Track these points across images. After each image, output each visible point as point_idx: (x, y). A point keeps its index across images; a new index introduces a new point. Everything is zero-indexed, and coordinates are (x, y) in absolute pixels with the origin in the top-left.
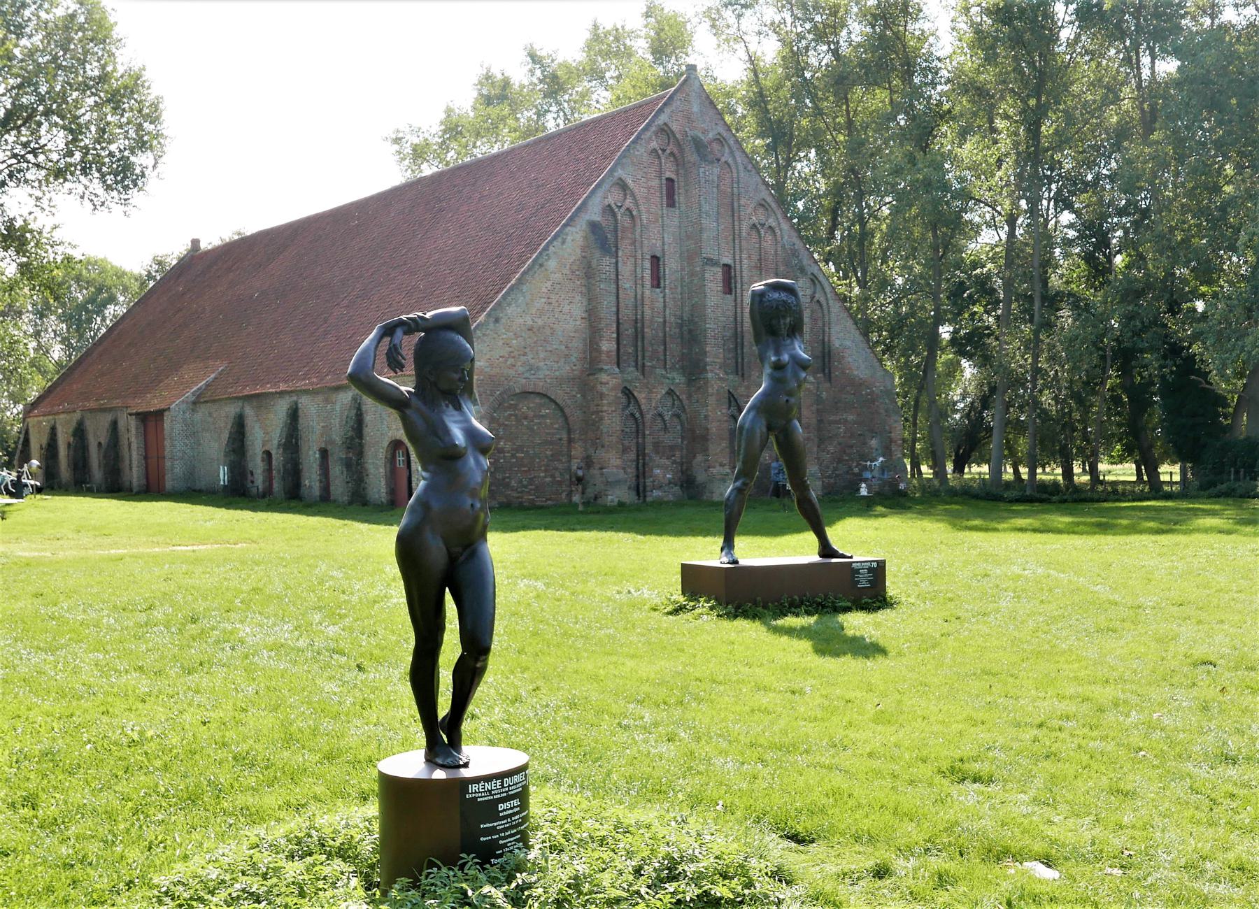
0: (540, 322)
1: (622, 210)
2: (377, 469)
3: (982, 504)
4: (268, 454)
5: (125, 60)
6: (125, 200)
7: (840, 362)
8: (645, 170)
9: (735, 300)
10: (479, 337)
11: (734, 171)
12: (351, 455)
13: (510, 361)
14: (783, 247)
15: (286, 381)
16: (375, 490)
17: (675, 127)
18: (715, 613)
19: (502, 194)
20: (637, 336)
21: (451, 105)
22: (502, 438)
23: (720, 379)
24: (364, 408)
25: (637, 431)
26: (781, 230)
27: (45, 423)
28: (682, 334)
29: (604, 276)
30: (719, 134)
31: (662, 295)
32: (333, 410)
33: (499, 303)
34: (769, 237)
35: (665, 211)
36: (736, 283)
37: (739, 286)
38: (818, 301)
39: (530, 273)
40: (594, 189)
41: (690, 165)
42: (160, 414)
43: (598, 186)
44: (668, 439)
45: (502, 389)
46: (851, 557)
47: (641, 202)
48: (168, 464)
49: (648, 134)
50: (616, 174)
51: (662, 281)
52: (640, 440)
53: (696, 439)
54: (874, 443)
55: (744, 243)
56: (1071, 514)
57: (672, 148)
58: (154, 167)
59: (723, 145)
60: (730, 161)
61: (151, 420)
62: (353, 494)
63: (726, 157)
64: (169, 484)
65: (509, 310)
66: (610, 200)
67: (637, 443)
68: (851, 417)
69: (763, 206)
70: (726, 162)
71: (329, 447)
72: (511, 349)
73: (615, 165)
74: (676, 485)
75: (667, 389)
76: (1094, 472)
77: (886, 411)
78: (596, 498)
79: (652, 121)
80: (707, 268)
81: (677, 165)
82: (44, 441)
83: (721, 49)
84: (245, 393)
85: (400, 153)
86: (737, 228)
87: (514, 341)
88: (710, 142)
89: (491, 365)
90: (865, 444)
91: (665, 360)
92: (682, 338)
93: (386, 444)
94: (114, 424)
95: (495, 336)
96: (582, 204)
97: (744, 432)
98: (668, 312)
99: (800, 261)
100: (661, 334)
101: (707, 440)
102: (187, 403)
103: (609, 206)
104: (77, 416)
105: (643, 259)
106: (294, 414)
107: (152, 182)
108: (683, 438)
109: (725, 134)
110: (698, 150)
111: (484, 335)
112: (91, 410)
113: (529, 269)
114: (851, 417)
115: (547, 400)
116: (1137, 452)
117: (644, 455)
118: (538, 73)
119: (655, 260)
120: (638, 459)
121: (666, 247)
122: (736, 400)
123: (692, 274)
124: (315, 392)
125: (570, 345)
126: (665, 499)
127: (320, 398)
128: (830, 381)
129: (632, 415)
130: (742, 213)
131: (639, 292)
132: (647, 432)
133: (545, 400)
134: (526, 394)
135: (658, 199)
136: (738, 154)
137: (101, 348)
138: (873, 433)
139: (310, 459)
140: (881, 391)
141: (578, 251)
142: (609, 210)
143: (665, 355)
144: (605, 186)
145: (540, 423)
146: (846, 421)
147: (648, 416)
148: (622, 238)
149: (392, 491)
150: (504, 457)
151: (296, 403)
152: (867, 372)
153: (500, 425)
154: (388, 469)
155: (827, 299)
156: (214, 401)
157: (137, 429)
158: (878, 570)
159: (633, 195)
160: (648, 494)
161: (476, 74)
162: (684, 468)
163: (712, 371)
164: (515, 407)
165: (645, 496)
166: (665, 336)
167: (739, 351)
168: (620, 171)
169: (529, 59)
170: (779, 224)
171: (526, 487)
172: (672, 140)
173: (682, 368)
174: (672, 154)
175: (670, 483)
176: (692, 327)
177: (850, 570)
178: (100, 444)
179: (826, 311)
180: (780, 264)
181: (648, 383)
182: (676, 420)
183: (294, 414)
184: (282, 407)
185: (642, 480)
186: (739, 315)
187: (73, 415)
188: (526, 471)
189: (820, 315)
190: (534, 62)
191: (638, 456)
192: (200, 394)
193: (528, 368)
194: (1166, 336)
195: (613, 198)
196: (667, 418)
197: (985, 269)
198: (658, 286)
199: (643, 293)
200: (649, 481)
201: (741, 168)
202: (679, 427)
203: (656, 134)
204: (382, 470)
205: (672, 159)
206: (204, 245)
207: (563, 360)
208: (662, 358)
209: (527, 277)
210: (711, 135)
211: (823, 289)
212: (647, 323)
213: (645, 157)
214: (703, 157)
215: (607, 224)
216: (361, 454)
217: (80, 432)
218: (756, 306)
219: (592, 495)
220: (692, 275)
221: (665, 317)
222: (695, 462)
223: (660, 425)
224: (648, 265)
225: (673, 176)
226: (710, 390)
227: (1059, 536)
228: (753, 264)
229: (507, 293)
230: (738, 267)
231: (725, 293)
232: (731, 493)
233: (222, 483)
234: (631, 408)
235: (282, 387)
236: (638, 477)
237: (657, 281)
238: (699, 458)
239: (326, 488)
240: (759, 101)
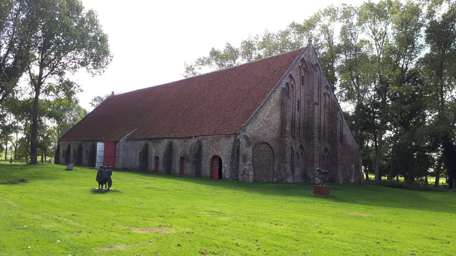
10: (251, 123)
14: (332, 101)
17: (305, 59)
26: (331, 95)
27: (67, 143)
29: (288, 105)
57: (304, 66)
66: (288, 81)
80: (315, 105)
81: (305, 72)
82: (66, 149)
86: (320, 93)
92: (304, 128)
93: (211, 157)
101: (314, 162)
109: (318, 63)
124: (180, 138)
125: (275, 128)
131: (294, 112)
132: (295, 158)
133: (267, 146)
134: (263, 143)
139: (177, 159)
153: (255, 153)
161: (210, 50)
164: (259, 147)
168: (291, 72)
170: (331, 93)
174: (304, 68)
178: (87, 151)
195: (288, 81)
201: (322, 74)
205: (303, 70)
220: (309, 107)
221: (300, 120)
224: (297, 103)
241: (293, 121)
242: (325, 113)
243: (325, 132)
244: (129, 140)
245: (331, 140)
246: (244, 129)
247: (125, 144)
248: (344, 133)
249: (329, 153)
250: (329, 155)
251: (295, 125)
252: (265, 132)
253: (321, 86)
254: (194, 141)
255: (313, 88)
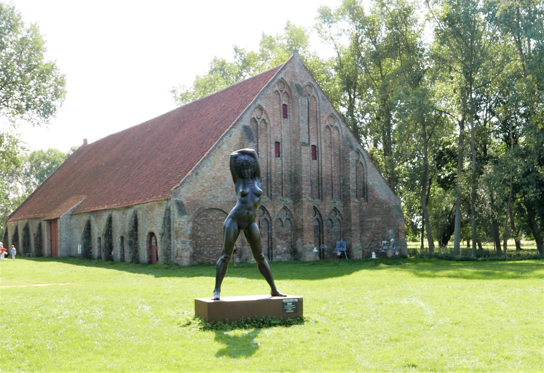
0: (219, 175)
1: (260, 120)
2: (143, 246)
3: (443, 262)
4: (100, 238)
5: (47, 58)
6: (47, 121)
7: (372, 192)
8: (272, 101)
9: (318, 162)
10: (188, 182)
11: (317, 100)
12: (132, 239)
13: (204, 194)
14: (342, 136)
15: (108, 204)
16: (143, 256)
17: (287, 80)
18: (199, 327)
19: (209, 114)
20: (268, 180)
21: (198, 75)
22: (199, 231)
23: (309, 201)
24: (138, 217)
25: (268, 228)
26: (341, 128)
28: (291, 180)
30: (309, 82)
31: (281, 161)
32: (126, 218)
33: (198, 166)
34: (335, 132)
35: (282, 120)
36: (318, 154)
37: (320, 156)
38: (361, 162)
39: (214, 151)
40: (246, 110)
41: (295, 97)
42: (56, 220)
43: (248, 109)
44: (284, 231)
45: (199, 207)
46: (285, 296)
47: (270, 116)
48: (59, 243)
49: (273, 83)
50: (257, 103)
51: (281, 154)
52: (270, 231)
53: (298, 230)
54: (390, 232)
55: (322, 135)
56: (475, 268)
57: (285, 89)
58: (61, 106)
59: (312, 88)
60: (315, 95)
61: (52, 222)
62: (133, 258)
63: (313, 93)
64: (59, 253)
65: (203, 169)
66: (254, 115)
67: (268, 233)
68: (378, 219)
69: (332, 116)
70: (313, 96)
71: (124, 236)
72: (204, 188)
73: (257, 99)
74: (288, 253)
75: (283, 206)
76: (518, 244)
77: (396, 216)
78: (246, 260)
79: (275, 77)
80: (303, 147)
81: (289, 98)
83: (323, 43)
84: (91, 210)
85: (175, 97)
86: (319, 127)
87: (206, 184)
88: (305, 86)
89: (194, 196)
90: (386, 232)
91: (282, 192)
93: (147, 234)
94: (40, 225)
95: (196, 181)
96: (240, 117)
97: (226, 230)
98: (283, 169)
99: (351, 143)
100: (280, 180)
102: (68, 215)
103: (254, 118)
104: (26, 221)
105: (271, 143)
106: (110, 220)
107: (59, 113)
108: (292, 230)
109: (312, 82)
110: (298, 90)
111: (191, 181)
112: (31, 219)
113: (213, 149)
114: (378, 219)
115: (222, 212)
116: (532, 234)
117: (272, 238)
118: (238, 57)
119: (277, 144)
120: (269, 240)
121: (283, 138)
122: (318, 211)
123: (296, 150)
126: (283, 260)
127: (121, 212)
128: (367, 201)
129: (266, 219)
130: (321, 120)
131: (269, 160)
132: (273, 227)
134: (211, 209)
135: (279, 114)
136: (319, 92)
137: (41, 190)
138: (390, 227)
139: (117, 241)
140: (394, 206)
141: (238, 140)
142: (254, 120)
143: (282, 190)
144: (252, 109)
145: (218, 223)
146: (376, 221)
147: (274, 220)
148: (261, 133)
149: (150, 257)
150: (201, 240)
151: (111, 215)
152: (386, 197)
154: (148, 246)
155: (365, 161)
156: (79, 214)
157: (47, 227)
158: (298, 304)
159: (266, 113)
160: (274, 257)
161: (211, 59)
162: (292, 245)
163: (305, 197)
165: (272, 259)
166: (282, 181)
167: (320, 187)
169: (234, 51)
171: (212, 254)
172: (286, 86)
173: (291, 196)
174: (286, 93)
175: (285, 252)
176: (296, 176)
177: (282, 304)
178: (34, 234)
179: (365, 167)
180: (341, 145)
181: (274, 203)
182: (288, 221)
183: (110, 220)
184: (105, 216)
185: (270, 251)
186: (320, 169)
187: (24, 221)
188: (211, 247)
189: (362, 169)
190: (236, 52)
191: (269, 239)
192: (74, 210)
193: (212, 197)
194: (537, 177)
196: (283, 220)
197: (451, 146)
198: (279, 156)
199: (271, 160)
200: (274, 251)
201: (321, 99)
202: (290, 225)
203: (278, 83)
204: (145, 247)
205: (286, 95)
206: (90, 142)
207: (230, 193)
208: (281, 191)
209: (212, 153)
210: (305, 83)
211: (363, 156)
212: (273, 174)
213: (272, 94)
214: (301, 94)
215: (252, 127)
216: (136, 239)
217: (26, 229)
218: (233, 162)
219: (245, 258)
220: (296, 151)
221: (282, 171)
222: (297, 242)
223: (280, 224)
224: (273, 146)
225: (286, 103)
226: (304, 207)
227: (468, 280)
228: (327, 145)
229: (202, 161)
230: (319, 146)
231: (313, 159)
232: (219, 262)
233: (79, 253)
234: (265, 215)
235: (106, 207)
236: (268, 249)
237: (278, 153)
238: (299, 240)
239: (123, 256)
240: (339, 67)
241: (268, 172)
242: (331, 156)
243: (332, 184)
244: (73, 215)
245: (343, 195)
246: (175, 193)
247: (68, 221)
248: (370, 183)
249: (340, 214)
250: (342, 218)
251: (271, 179)
252: (214, 194)
253: (320, 117)
254: (130, 212)
255: (299, 122)
